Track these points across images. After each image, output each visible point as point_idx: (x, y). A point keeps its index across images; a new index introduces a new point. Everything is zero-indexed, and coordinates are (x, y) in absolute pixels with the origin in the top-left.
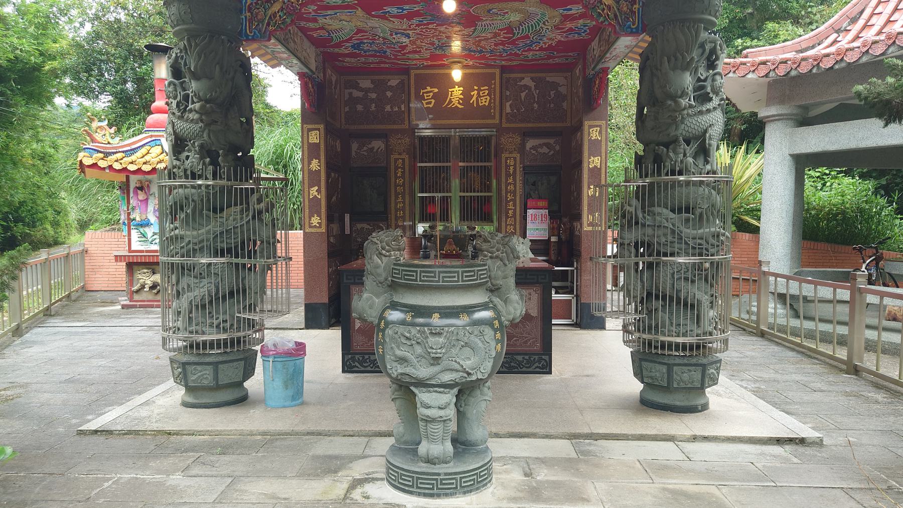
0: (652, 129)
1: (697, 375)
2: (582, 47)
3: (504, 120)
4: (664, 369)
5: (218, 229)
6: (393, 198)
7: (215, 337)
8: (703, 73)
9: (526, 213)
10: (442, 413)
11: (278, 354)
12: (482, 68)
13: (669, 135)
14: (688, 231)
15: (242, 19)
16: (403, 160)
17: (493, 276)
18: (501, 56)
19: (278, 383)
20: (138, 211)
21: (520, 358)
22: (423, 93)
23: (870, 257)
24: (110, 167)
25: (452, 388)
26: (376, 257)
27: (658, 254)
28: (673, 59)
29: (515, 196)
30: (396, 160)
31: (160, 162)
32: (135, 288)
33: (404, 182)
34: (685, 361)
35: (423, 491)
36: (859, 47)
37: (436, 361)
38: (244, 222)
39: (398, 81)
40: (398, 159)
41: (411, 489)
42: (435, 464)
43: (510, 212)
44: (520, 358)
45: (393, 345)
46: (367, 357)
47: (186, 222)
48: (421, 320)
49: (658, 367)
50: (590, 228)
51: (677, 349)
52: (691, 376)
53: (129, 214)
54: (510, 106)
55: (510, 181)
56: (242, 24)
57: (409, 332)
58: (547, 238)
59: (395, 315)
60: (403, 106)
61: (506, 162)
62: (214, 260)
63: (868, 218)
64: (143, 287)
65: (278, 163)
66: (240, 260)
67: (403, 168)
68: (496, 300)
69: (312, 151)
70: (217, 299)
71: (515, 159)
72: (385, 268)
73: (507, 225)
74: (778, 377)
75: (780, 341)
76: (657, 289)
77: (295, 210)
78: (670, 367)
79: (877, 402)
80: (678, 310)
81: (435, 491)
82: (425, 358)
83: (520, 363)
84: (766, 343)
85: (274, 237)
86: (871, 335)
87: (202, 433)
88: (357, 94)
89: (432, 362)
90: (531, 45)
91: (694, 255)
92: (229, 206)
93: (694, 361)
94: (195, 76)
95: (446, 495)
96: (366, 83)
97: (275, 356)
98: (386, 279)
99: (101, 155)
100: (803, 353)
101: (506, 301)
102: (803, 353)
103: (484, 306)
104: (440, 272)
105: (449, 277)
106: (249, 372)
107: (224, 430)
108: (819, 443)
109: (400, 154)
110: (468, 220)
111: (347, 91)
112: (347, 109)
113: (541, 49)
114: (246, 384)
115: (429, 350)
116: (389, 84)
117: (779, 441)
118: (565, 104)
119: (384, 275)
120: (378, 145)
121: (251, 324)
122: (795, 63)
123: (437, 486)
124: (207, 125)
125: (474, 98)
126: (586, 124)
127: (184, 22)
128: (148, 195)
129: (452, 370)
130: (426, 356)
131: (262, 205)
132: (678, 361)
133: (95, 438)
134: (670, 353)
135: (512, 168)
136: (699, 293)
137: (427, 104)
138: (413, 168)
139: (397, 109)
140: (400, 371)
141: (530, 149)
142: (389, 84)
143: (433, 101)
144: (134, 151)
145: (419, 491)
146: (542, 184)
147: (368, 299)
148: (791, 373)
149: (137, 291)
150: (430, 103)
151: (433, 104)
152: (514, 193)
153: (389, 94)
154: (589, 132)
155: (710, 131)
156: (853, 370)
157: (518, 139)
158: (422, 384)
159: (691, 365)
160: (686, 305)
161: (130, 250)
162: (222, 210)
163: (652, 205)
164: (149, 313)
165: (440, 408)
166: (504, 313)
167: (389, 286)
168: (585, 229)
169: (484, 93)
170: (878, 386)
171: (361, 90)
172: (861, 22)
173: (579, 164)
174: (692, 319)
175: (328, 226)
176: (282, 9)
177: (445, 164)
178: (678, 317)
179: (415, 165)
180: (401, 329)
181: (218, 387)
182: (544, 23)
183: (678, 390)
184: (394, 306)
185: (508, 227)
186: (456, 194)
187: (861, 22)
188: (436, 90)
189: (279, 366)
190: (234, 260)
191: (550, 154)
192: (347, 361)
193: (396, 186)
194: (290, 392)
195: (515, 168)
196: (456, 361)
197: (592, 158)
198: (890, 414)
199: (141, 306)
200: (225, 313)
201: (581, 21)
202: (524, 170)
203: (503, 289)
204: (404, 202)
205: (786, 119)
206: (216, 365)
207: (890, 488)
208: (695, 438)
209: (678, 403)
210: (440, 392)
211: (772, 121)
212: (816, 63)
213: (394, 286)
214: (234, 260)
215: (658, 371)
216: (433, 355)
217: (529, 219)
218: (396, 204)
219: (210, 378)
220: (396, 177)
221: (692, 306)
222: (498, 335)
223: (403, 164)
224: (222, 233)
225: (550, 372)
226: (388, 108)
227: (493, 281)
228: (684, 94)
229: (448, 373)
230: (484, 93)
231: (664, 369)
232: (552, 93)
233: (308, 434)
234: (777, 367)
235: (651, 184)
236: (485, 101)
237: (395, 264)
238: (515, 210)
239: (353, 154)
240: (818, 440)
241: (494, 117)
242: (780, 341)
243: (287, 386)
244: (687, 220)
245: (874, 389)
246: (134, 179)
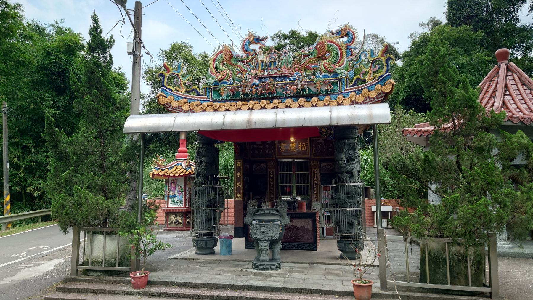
6: (269, 186)
7: (206, 232)
8: (351, 152)
10: (265, 248)
11: (224, 238)
16: (273, 171)
19: (224, 247)
20: (172, 191)
21: (306, 245)
24: (164, 175)
29: (317, 185)
31: (182, 172)
32: (169, 222)
37: (263, 233)
38: (397, 293)
44: (306, 245)
47: (199, 198)
48: (261, 223)
51: (350, 239)
53: (168, 193)
55: (315, 179)
59: (255, 222)
62: (206, 209)
64: (172, 222)
65: (225, 169)
66: (214, 209)
68: (281, 219)
69: (238, 169)
70: (207, 221)
71: (317, 170)
76: (341, 219)
77: (232, 189)
78: (345, 244)
80: (348, 225)
83: (306, 246)
85: (224, 202)
88: (255, 146)
91: (352, 208)
92: (211, 192)
94: (204, 156)
99: (161, 170)
106: (215, 245)
111: (252, 145)
112: (252, 152)
119: (252, 212)
120: (263, 166)
121: (216, 228)
124: (206, 169)
127: (201, 140)
128: (176, 185)
131: (221, 192)
133: (173, 260)
138: (277, 174)
139: (270, 152)
144: (171, 168)
149: (170, 224)
153: (267, 146)
158: (260, 240)
161: (168, 207)
162: (209, 194)
164: (175, 232)
171: (257, 145)
174: (352, 228)
175: (243, 198)
178: (348, 228)
179: (278, 173)
180: (255, 226)
181: (206, 248)
184: (254, 220)
189: (225, 242)
190: (212, 209)
193: (270, 182)
194: (228, 250)
195: (317, 174)
199: (171, 230)
200: (209, 225)
204: (273, 188)
206: (206, 241)
213: (254, 215)
214: (212, 209)
219: (204, 245)
220: (270, 178)
221: (352, 224)
222: (281, 228)
225: (316, 250)
226: (267, 152)
233: (233, 260)
235: (336, 186)
241: (308, 155)
246: (171, 179)
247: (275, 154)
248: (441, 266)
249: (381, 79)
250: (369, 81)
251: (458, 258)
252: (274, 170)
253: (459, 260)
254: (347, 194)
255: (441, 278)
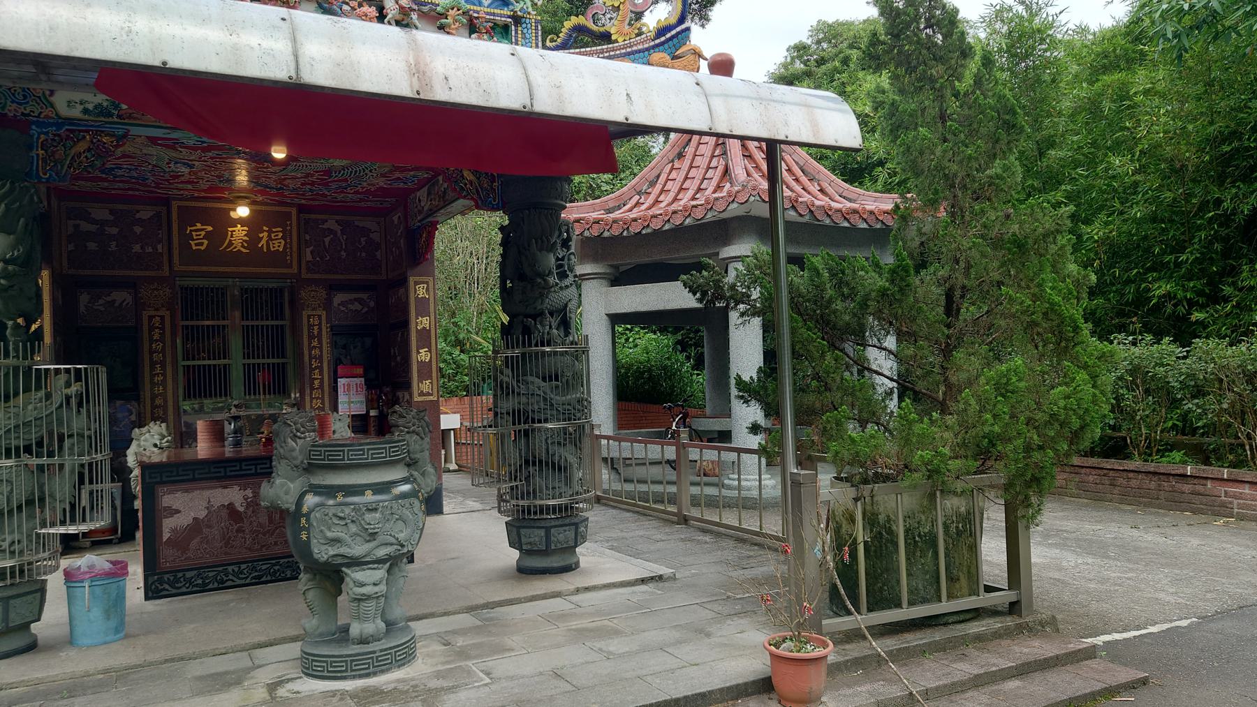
0: (520, 302)
1: (571, 534)
2: (403, 197)
3: (303, 271)
4: (542, 532)
5: (12, 421)
6: (147, 369)
9: (336, 382)
10: (376, 589)
12: (275, 205)
13: (536, 308)
14: (558, 398)
15: (33, 157)
16: (162, 318)
17: (411, 450)
18: (303, 195)
22: (191, 230)
23: (678, 416)
25: (385, 563)
26: (290, 440)
27: (533, 422)
28: (540, 241)
29: (321, 362)
30: (151, 318)
33: (164, 348)
34: (560, 522)
35: (358, 673)
36: (661, 215)
39: (152, 214)
40: (154, 316)
41: (344, 674)
42: (368, 643)
43: (316, 382)
45: (323, 528)
46: (180, 575)
49: (537, 532)
50: (420, 399)
52: (568, 534)
54: (312, 252)
55: (315, 343)
56: (32, 163)
57: (342, 511)
58: (364, 413)
60: (159, 247)
61: (309, 321)
63: (671, 376)
67: (163, 329)
68: (415, 474)
72: (301, 451)
73: (312, 399)
74: (624, 534)
75: (615, 504)
79: (706, 543)
81: (372, 669)
82: (360, 536)
84: (604, 508)
86: (695, 490)
87: (15, 685)
88: (85, 226)
89: (368, 539)
90: (346, 189)
92: (27, 389)
93: (567, 521)
95: (382, 672)
96: (100, 212)
97: (93, 578)
98: (302, 462)
100: (638, 512)
101: (423, 474)
102: (638, 512)
103: (405, 481)
104: (368, 450)
105: (378, 453)
107: (48, 677)
108: (673, 578)
109: (157, 310)
110: (195, 397)
111: (71, 223)
112: (71, 247)
113: (357, 193)
114: (34, 627)
115: (367, 527)
116: (138, 216)
117: (643, 581)
118: (378, 254)
119: (300, 458)
120: (121, 297)
122: (607, 225)
123: (373, 663)
125: (264, 242)
126: (412, 280)
129: (386, 544)
130: (362, 534)
132: (553, 523)
134: (542, 517)
135: (316, 328)
136: (567, 454)
137: (196, 245)
140: (332, 553)
141: (339, 305)
142: (138, 216)
143: (206, 242)
145: (354, 673)
146: (355, 348)
147: (282, 485)
148: (635, 530)
150: (202, 244)
151: (205, 246)
152: (320, 358)
153: (138, 230)
154: (415, 289)
155: (570, 306)
156: (683, 521)
157: (323, 293)
158: (356, 563)
159: (566, 525)
160: (560, 469)
163: (525, 374)
165: (375, 584)
166: (423, 486)
167: (304, 469)
168: (416, 399)
169: (277, 235)
170: (704, 531)
171: (94, 222)
172: (658, 187)
173: (405, 324)
176: (89, 150)
177: (221, 323)
178: (554, 479)
182: (371, 171)
183: (555, 552)
185: (314, 401)
186: (237, 362)
187: (658, 187)
188: (210, 228)
189: (98, 590)
191: (363, 312)
192: (152, 584)
193: (151, 352)
194: (113, 623)
195: (320, 329)
196: (391, 535)
197: (420, 319)
198: (717, 550)
201: (412, 173)
202: (331, 330)
203: (420, 463)
204: (164, 375)
205: (600, 278)
207: (728, 597)
208: (578, 591)
209: (555, 565)
210: (374, 569)
211: (587, 279)
212: (626, 226)
215: (536, 536)
216: (371, 531)
217: (340, 390)
218: (152, 376)
220: (151, 341)
221: (565, 468)
223: (163, 322)
224: (17, 427)
227: (411, 455)
228: (550, 273)
229: (382, 547)
230: (277, 235)
231: (542, 532)
232: (362, 239)
233: (166, 661)
234: (621, 526)
236: (278, 245)
237: (313, 446)
238: (322, 380)
239: (82, 309)
240: (672, 575)
241: (290, 266)
242: (615, 504)
243: (109, 615)
244: (557, 387)
245: (701, 533)
247: (170, 261)
248: (918, 554)
249: (668, 35)
250: (620, 40)
251: (957, 527)
252: (167, 314)
253: (959, 533)
254: (551, 380)
255: (920, 586)
